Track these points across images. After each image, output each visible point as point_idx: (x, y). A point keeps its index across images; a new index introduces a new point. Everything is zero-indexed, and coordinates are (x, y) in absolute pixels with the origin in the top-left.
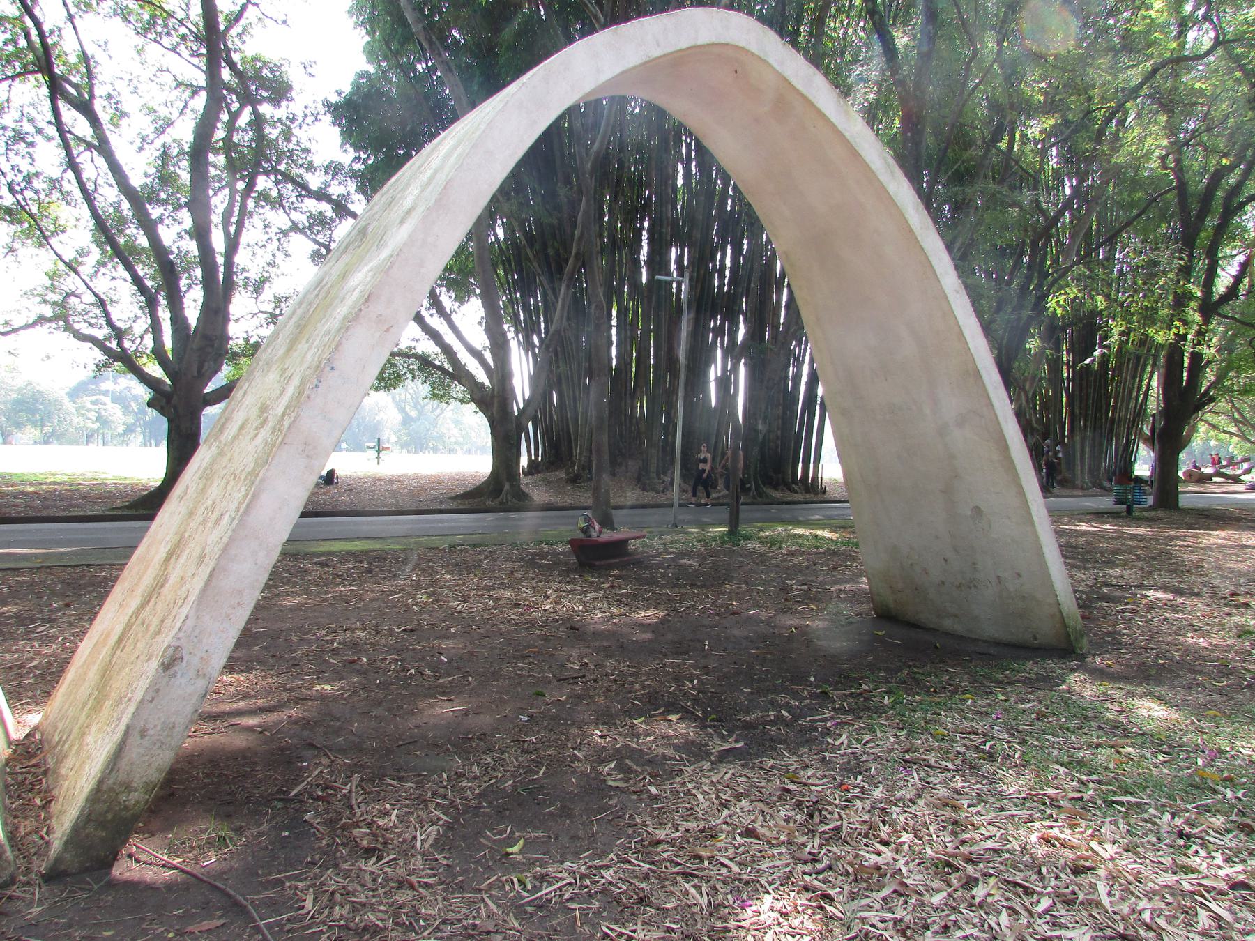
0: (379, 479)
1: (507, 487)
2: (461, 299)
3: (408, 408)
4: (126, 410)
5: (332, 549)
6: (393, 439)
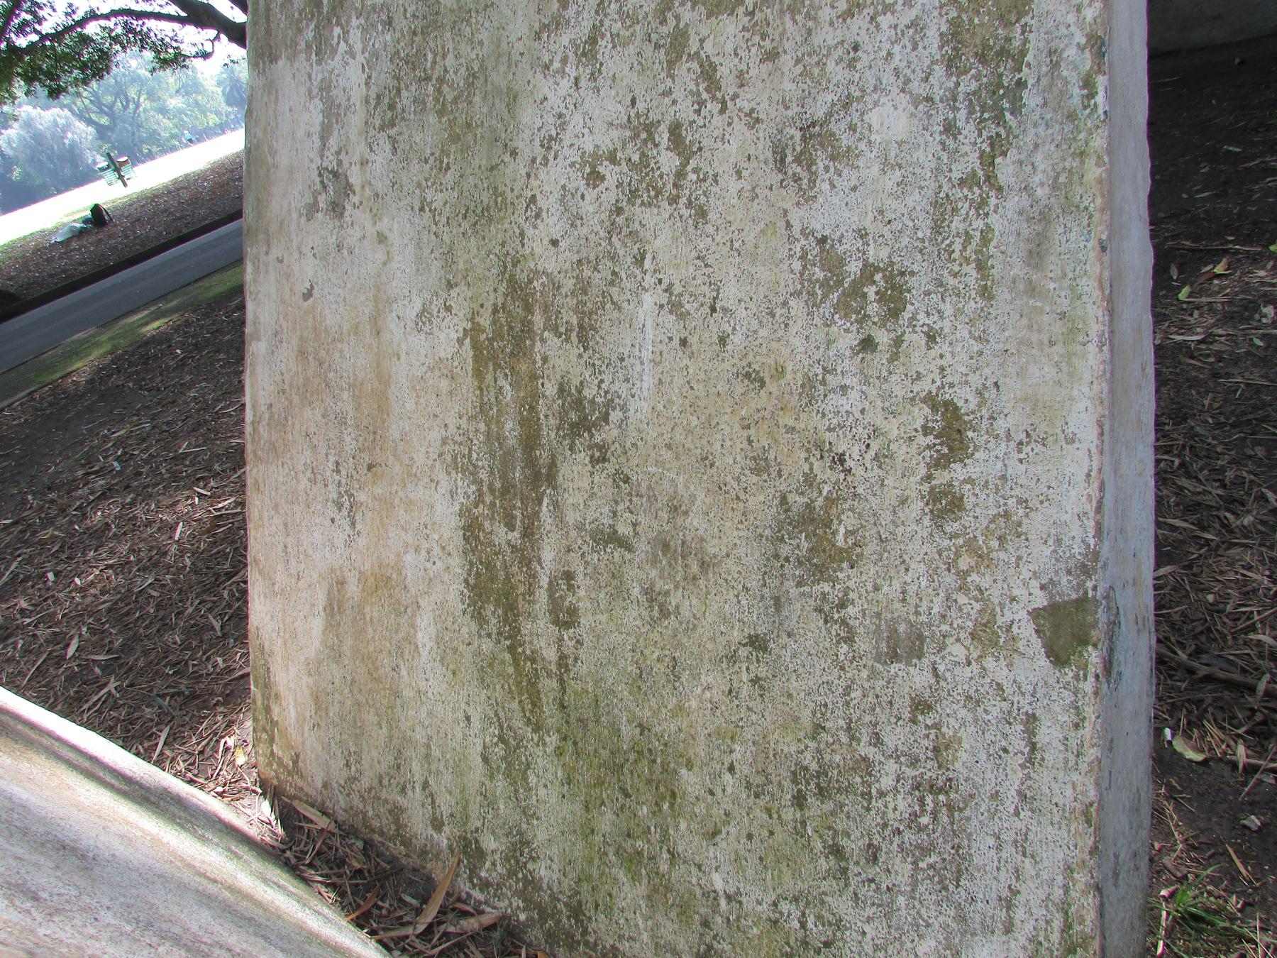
0: (156, 196)
3: (93, 117)
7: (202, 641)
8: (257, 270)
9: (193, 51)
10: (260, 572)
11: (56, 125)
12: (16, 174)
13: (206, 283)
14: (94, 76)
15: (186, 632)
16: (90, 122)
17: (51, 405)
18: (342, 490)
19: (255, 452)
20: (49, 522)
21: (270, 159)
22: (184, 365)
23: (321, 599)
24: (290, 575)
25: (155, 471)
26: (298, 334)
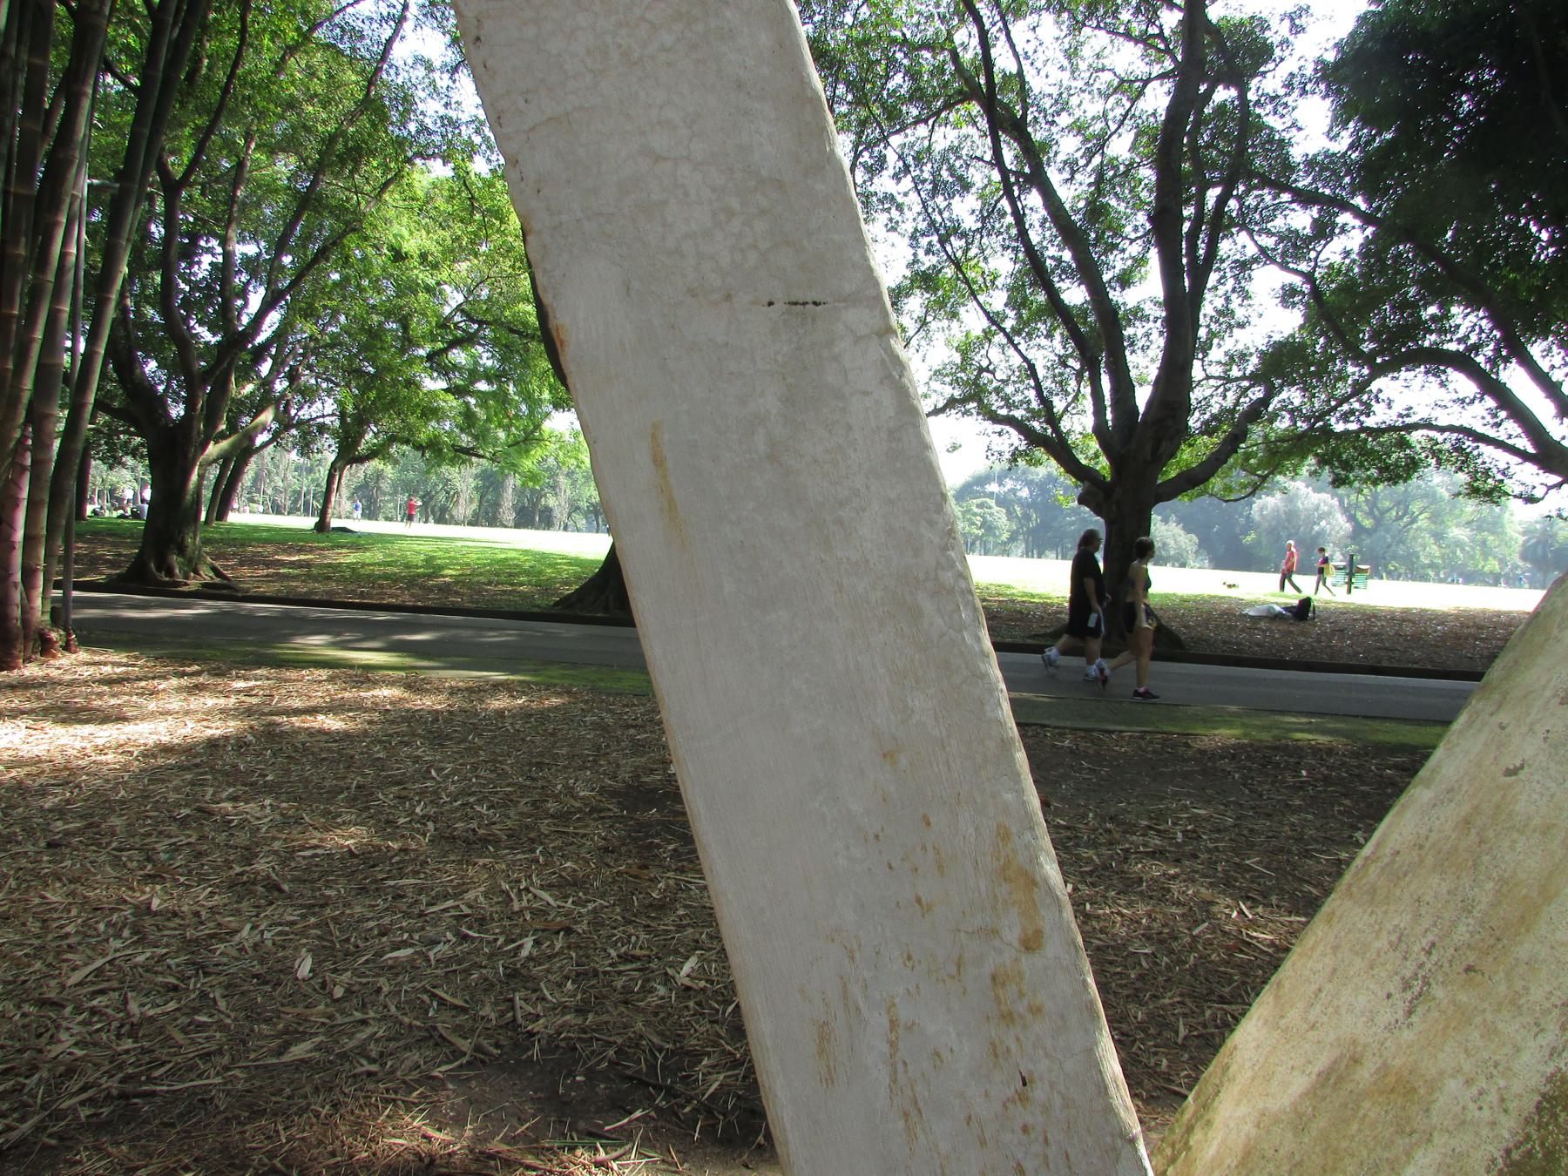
0: (1375, 616)
3: (1359, 515)
4: (1010, 514)
7: (1160, 1034)
8: (1470, 724)
9: (1518, 490)
10: (1277, 997)
11: (1317, 508)
12: (1250, 538)
13: (1375, 724)
14: (1389, 480)
15: (1151, 1016)
16: (1352, 518)
17: (1155, 751)
18: (1421, 973)
19: (1350, 886)
20: (1093, 844)
21: (1555, 632)
22: (1301, 788)
23: (1322, 1062)
24: (1305, 1020)
25: (1212, 864)
26: (1475, 802)
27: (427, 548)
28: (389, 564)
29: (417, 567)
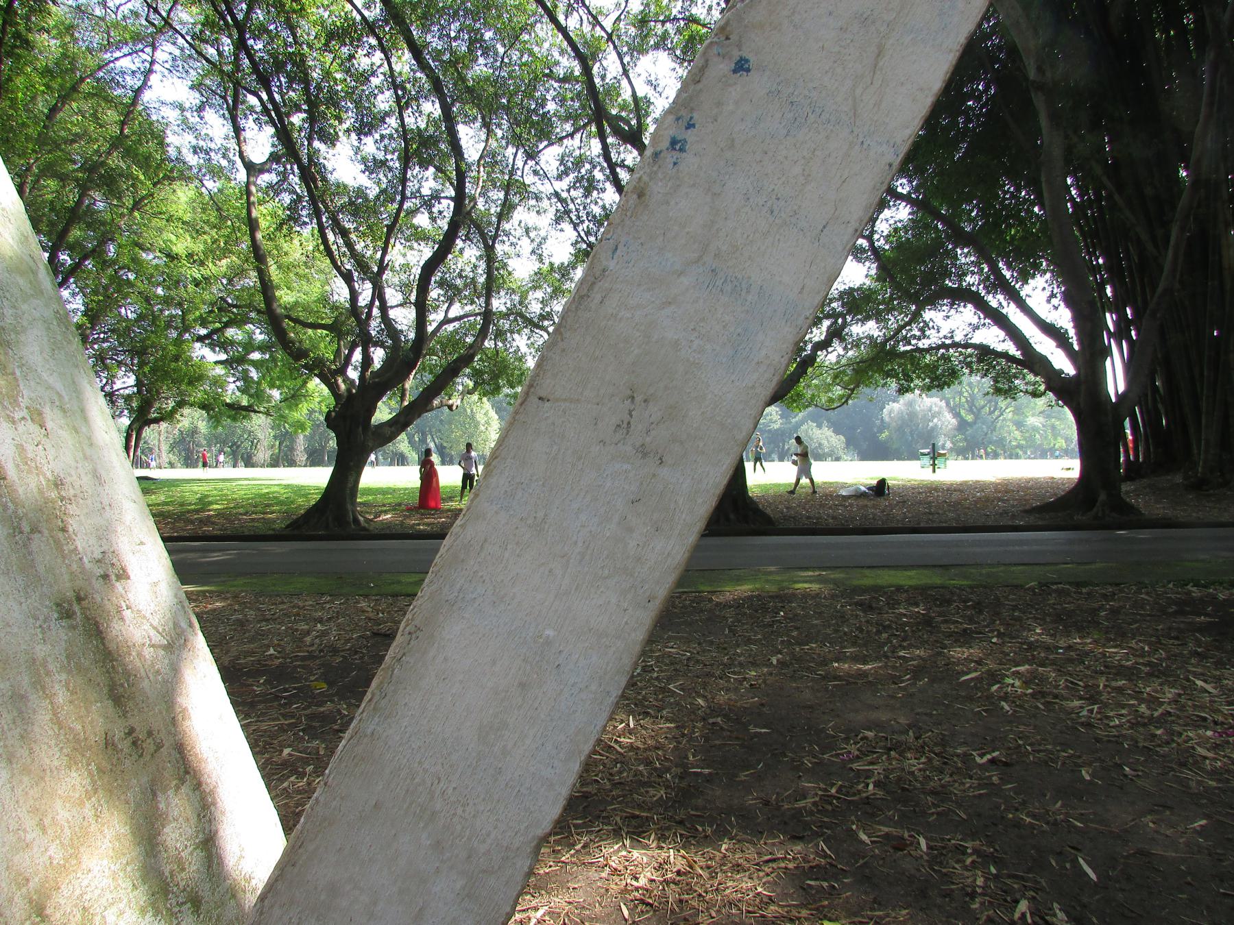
1: (1103, 497)
2: (1025, 277)
3: (963, 413)
5: (880, 582)
6: (949, 445)
14: (938, 386)
16: (957, 415)
27: (204, 489)
28: (167, 504)
29: (190, 504)
